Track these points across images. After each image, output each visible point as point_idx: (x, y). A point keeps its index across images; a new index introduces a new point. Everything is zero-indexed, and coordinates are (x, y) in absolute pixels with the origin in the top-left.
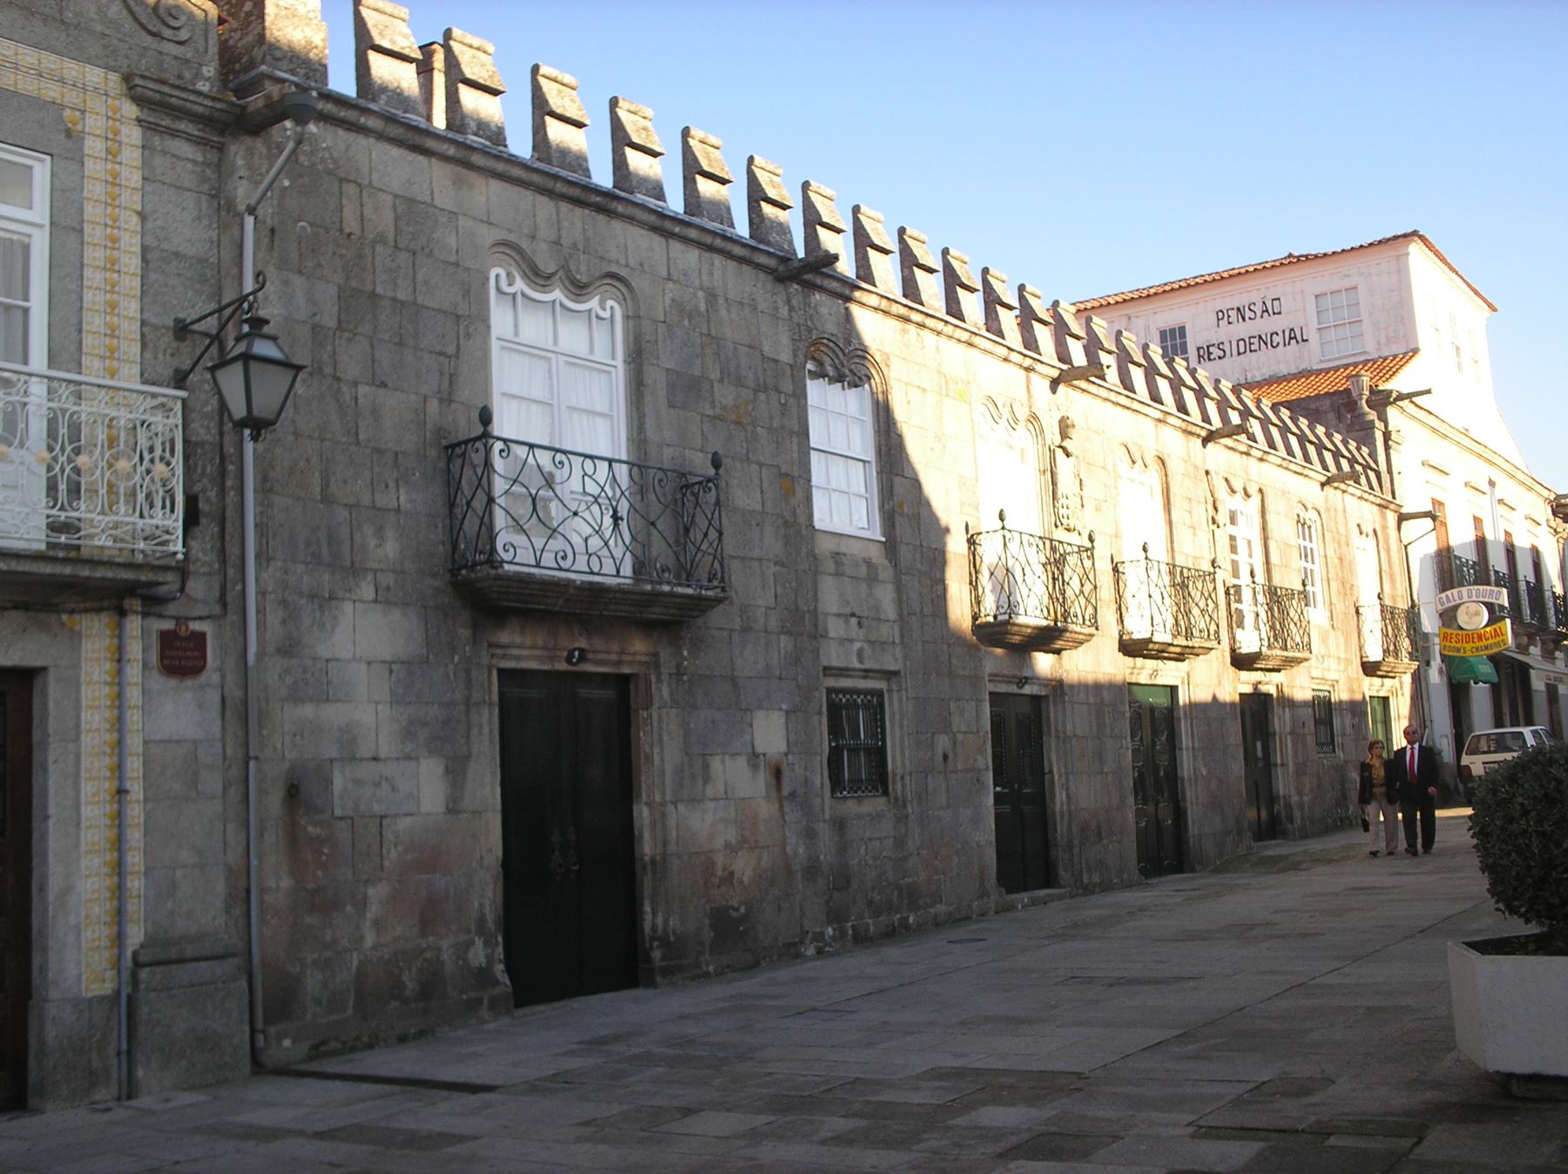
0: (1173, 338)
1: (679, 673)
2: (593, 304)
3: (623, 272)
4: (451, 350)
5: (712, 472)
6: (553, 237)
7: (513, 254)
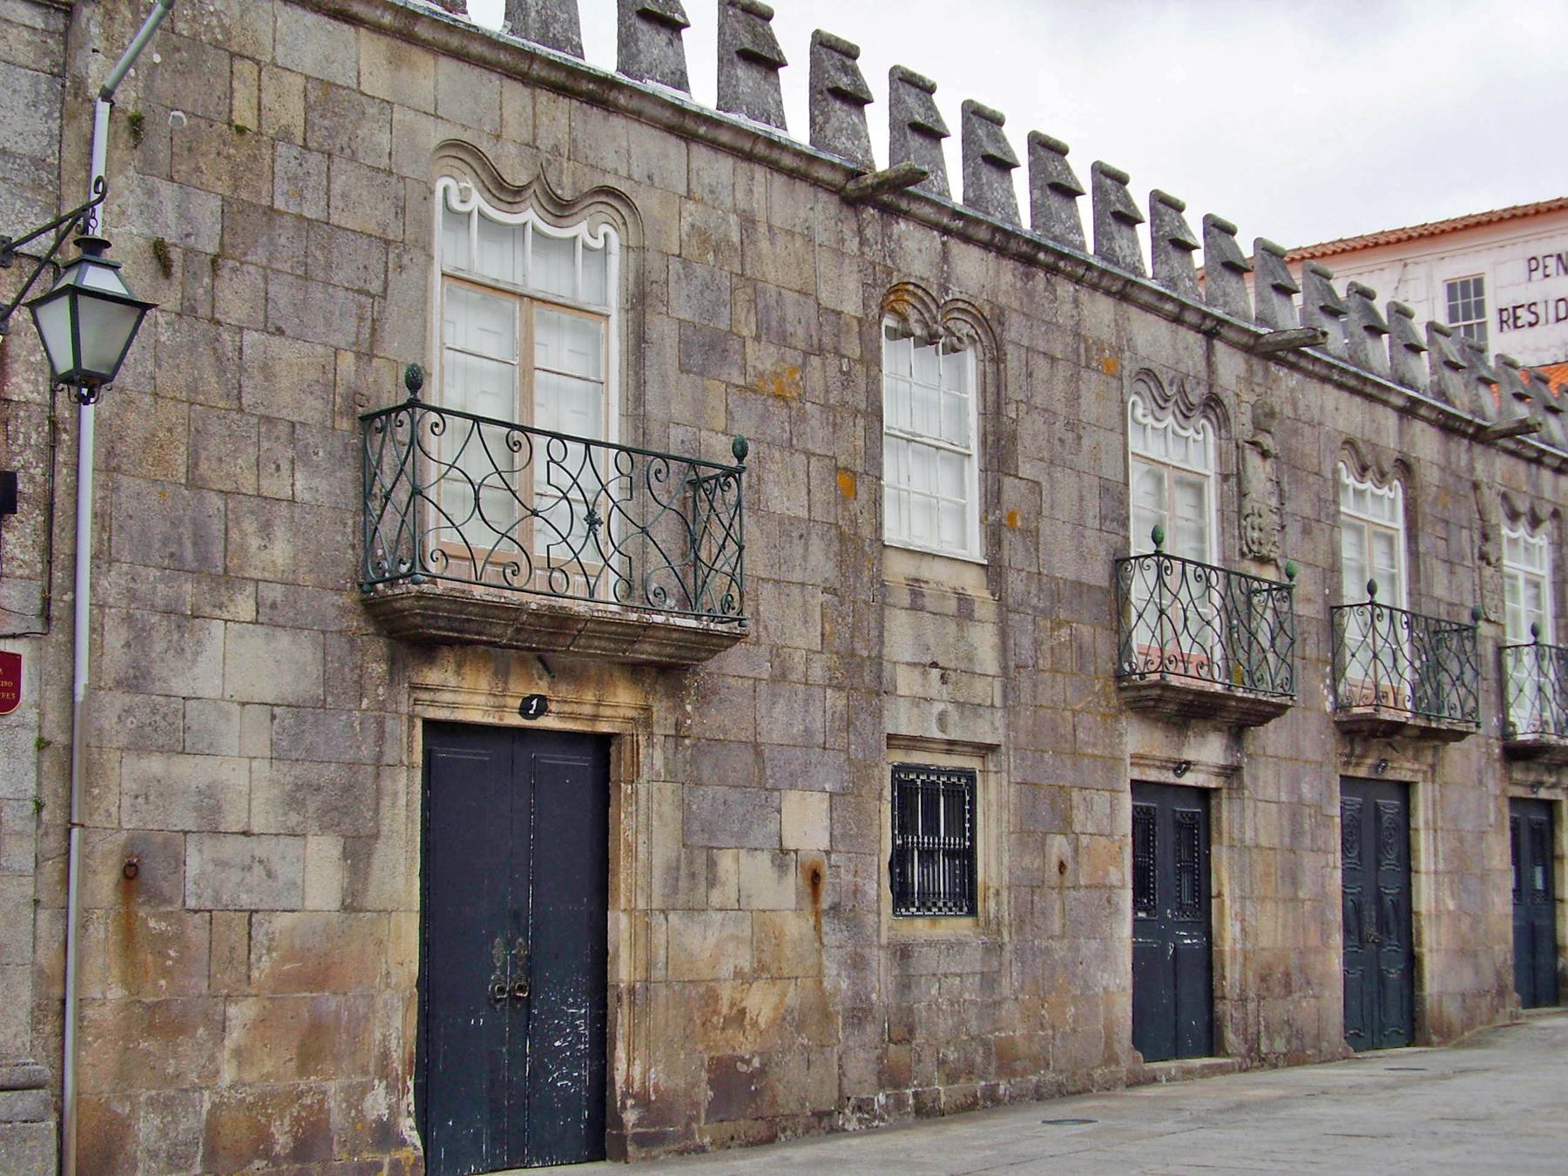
0: (1465, 295)
1: (678, 736)
2: (579, 229)
3: (623, 187)
4: (375, 286)
5: (734, 463)
6: (527, 137)
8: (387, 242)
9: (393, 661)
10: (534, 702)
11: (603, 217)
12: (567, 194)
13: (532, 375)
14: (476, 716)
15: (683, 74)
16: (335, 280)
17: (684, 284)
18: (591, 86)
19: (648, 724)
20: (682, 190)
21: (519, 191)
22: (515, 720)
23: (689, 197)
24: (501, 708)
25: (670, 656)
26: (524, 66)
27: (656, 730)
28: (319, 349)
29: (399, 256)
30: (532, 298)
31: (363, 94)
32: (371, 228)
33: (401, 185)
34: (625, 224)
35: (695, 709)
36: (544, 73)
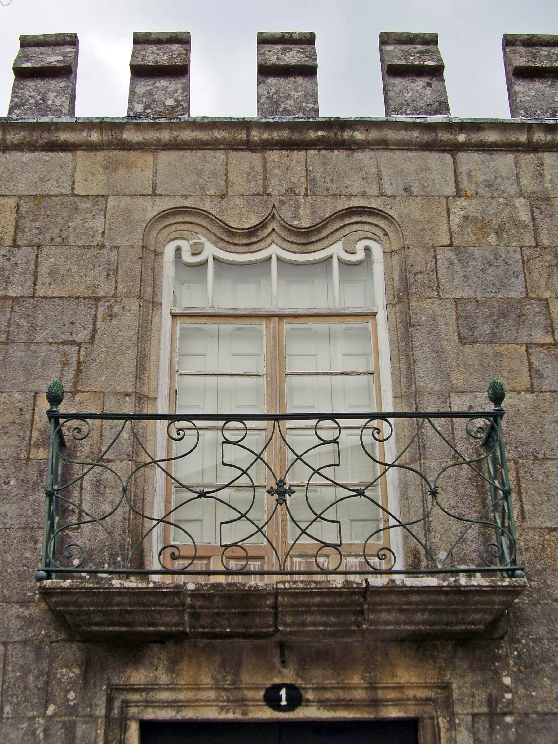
1: (494, 714)
3: (374, 204)
4: (82, 336)
6: (256, 187)
7: (172, 220)
8: (97, 299)
9: (87, 666)
10: (283, 692)
11: (360, 234)
12: (449, 243)
13: (283, 382)
14: (211, 714)
15: (446, 104)
16: (39, 338)
17: (458, 267)
18: (320, 133)
19: (448, 704)
20: (450, 190)
21: (252, 232)
22: (266, 714)
23: (459, 193)
24: (241, 702)
25: (424, 623)
26: (242, 136)
27: (458, 709)
28: (17, 396)
29: (110, 308)
30: (281, 317)
31: (76, 196)
32: (82, 291)
33: (115, 252)
34: (386, 234)
35: (516, 680)
36: (265, 136)
